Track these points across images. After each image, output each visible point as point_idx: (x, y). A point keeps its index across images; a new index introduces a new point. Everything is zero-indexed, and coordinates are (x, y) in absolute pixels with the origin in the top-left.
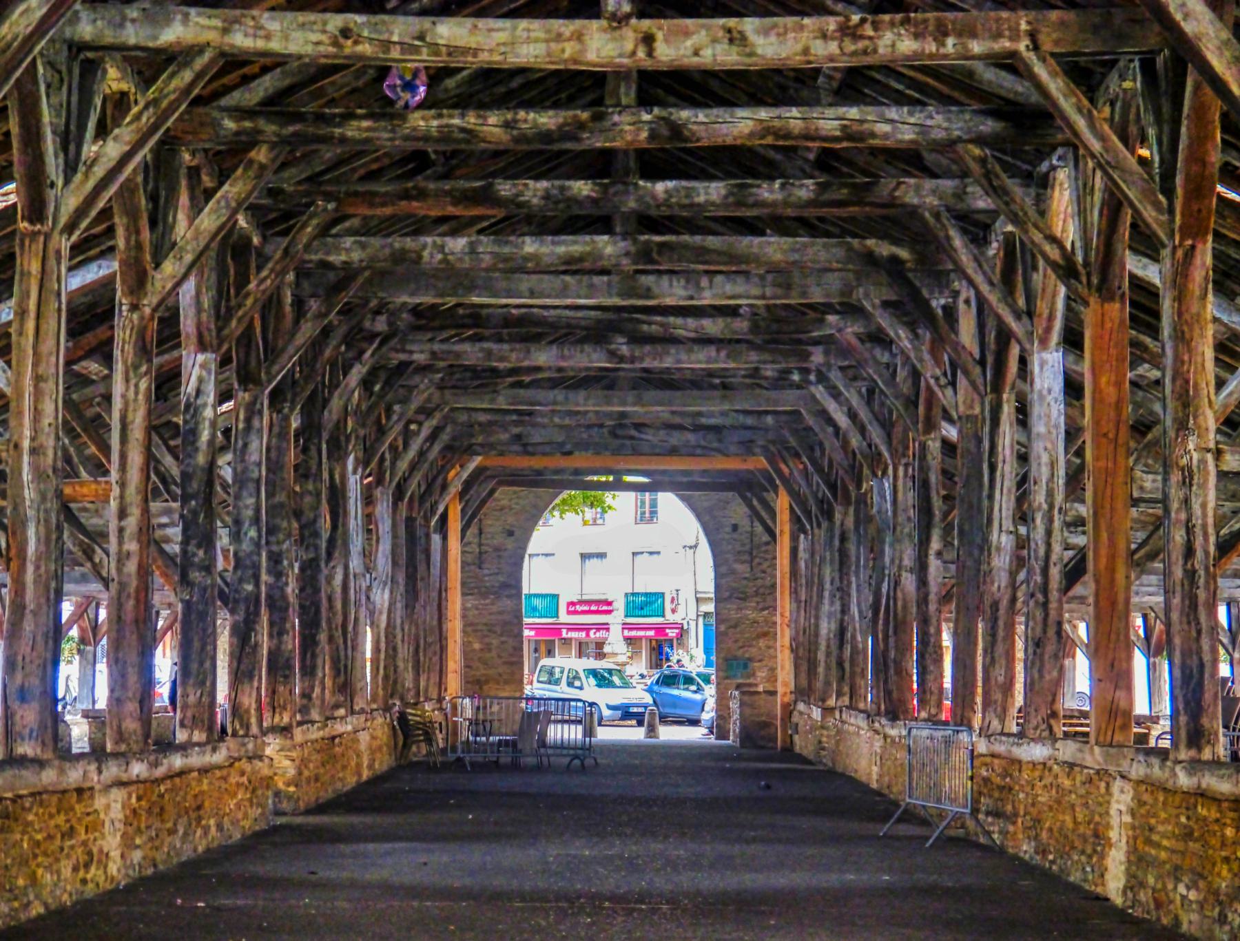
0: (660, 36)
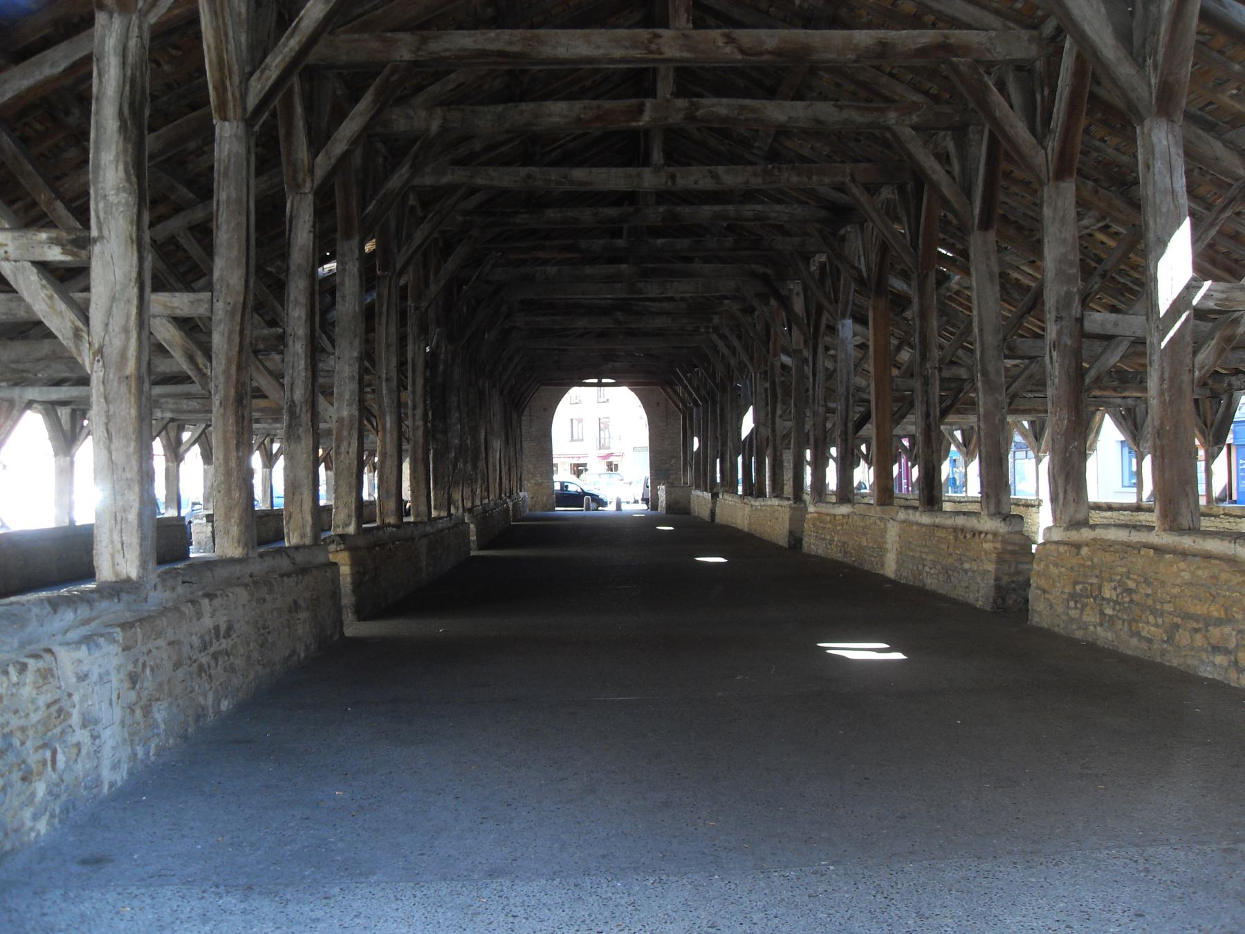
0: (678, 175)
